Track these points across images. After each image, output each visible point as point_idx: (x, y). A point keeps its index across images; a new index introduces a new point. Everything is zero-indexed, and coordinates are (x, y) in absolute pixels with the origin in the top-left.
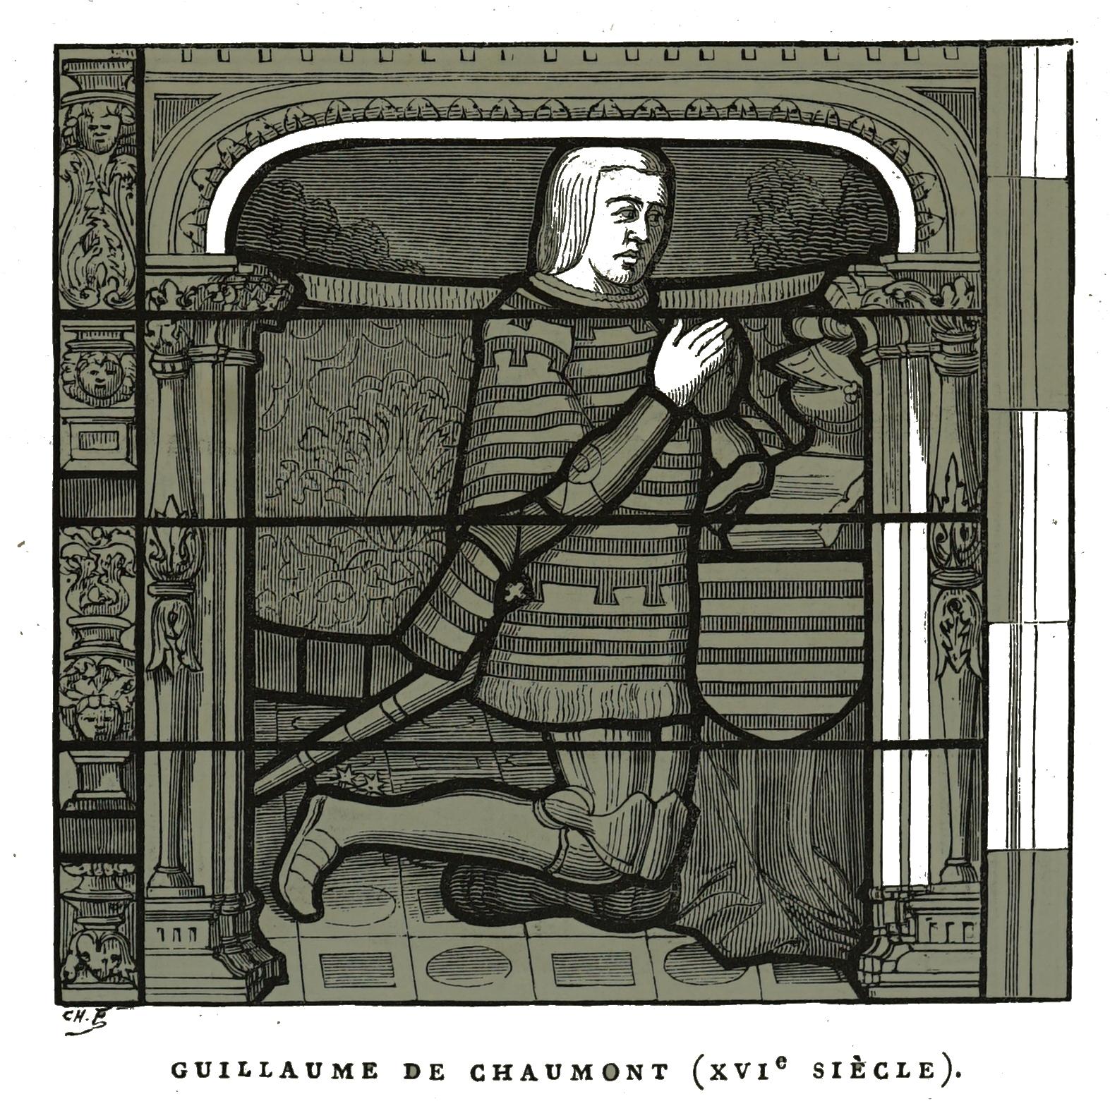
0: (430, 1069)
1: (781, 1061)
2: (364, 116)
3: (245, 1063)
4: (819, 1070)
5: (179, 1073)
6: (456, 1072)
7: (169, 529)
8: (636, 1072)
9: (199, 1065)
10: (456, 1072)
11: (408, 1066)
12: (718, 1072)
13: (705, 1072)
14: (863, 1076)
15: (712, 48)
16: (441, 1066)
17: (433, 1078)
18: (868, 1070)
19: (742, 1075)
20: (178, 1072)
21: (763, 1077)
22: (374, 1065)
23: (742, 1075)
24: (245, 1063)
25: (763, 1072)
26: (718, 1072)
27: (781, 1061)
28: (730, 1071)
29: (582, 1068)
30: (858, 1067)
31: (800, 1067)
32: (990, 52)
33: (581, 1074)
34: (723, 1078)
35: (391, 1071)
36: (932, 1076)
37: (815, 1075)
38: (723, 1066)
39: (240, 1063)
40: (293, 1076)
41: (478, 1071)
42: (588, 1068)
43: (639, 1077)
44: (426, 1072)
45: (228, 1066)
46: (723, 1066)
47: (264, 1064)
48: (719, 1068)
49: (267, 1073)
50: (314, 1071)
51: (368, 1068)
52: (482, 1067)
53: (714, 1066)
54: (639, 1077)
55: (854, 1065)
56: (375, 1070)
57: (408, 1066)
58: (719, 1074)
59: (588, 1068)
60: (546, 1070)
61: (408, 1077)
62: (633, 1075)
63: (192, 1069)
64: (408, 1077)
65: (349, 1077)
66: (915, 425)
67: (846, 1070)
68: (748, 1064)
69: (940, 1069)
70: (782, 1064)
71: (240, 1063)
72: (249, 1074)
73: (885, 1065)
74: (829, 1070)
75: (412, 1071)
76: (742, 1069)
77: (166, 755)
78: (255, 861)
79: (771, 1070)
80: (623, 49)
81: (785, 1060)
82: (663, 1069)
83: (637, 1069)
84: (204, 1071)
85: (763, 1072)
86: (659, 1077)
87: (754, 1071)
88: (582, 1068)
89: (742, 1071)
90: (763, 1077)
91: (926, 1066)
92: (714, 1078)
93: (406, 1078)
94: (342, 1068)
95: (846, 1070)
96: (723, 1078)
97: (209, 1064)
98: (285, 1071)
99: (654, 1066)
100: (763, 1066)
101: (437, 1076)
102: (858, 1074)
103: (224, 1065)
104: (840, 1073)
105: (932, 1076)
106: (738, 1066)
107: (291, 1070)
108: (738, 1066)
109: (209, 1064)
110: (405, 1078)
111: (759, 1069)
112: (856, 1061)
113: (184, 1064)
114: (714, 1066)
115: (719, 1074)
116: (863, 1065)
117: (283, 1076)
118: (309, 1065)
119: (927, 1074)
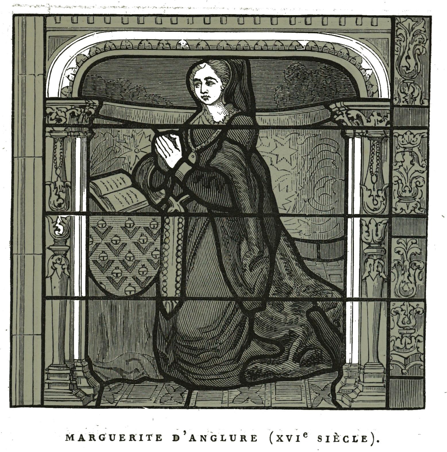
0: (251, 437)
1: (305, 434)
2: (236, 48)
3: (355, 436)
4: (320, 438)
5: (102, 439)
6: (263, 438)
7: (146, 200)
8: (203, 438)
9: (110, 435)
10: (263, 438)
11: (174, 436)
12: (280, 438)
13: (274, 438)
14: (339, 441)
15: (127, 17)
16: (124, 435)
17: (121, 440)
18: (341, 439)
19: (289, 440)
20: (71, 437)
21: (298, 441)
22: (161, 435)
23: (289, 440)
24: (355, 436)
25: (328, 439)
26: (280, 438)
27: (305, 434)
28: (284, 438)
29: (70, 436)
30: (336, 437)
31: (313, 437)
32: (48, 19)
33: (69, 438)
34: (282, 441)
35: (167, 438)
36: (256, 440)
37: (318, 441)
38: (282, 436)
39: (353, 436)
40: (194, 440)
41: (346, 438)
42: (72, 436)
43: (205, 440)
44: (118, 438)
45: (329, 437)
46: (282, 436)
47: (222, 436)
48: (280, 437)
49: (356, 440)
50: (233, 438)
51: (158, 437)
52: (347, 437)
53: (278, 436)
54: (205, 440)
55: (335, 436)
56: (161, 437)
57: (174, 436)
58: (280, 439)
59: (72, 436)
60: (230, 437)
61: (174, 440)
62: (203, 439)
63: (107, 437)
64: (174, 440)
65: (73, 440)
66: (149, 185)
67: (331, 439)
68: (291, 436)
69: (369, 438)
70: (306, 436)
71: (353, 436)
72: (357, 441)
73: (347, 437)
74: (324, 439)
75: (158, 437)
76: (289, 437)
77: (77, 294)
78: (290, 355)
79: (301, 438)
80: (154, 17)
81: (307, 434)
82: (150, 436)
83: (204, 437)
84: (233, 439)
85: (328, 439)
86: (149, 440)
87: (294, 438)
88: (70, 436)
89: (289, 438)
90: (298, 441)
91: (122, 436)
92: (278, 441)
93: (173, 441)
94: (70, 436)
95: (331, 439)
96: (282, 441)
97: (114, 435)
98: (191, 438)
99: (147, 435)
100: (298, 436)
101: (122, 439)
102: (159, 439)
103: (328, 437)
104: (326, 438)
105: (161, 440)
106: (288, 436)
107: (193, 438)
108: (288, 436)
109: (114, 435)
110: (173, 441)
111: (297, 437)
112: (335, 435)
113: (215, 436)
114: (278, 436)
115: (280, 439)
116: (338, 436)
117: (79, 440)
118: (231, 436)
119: (254, 440)
